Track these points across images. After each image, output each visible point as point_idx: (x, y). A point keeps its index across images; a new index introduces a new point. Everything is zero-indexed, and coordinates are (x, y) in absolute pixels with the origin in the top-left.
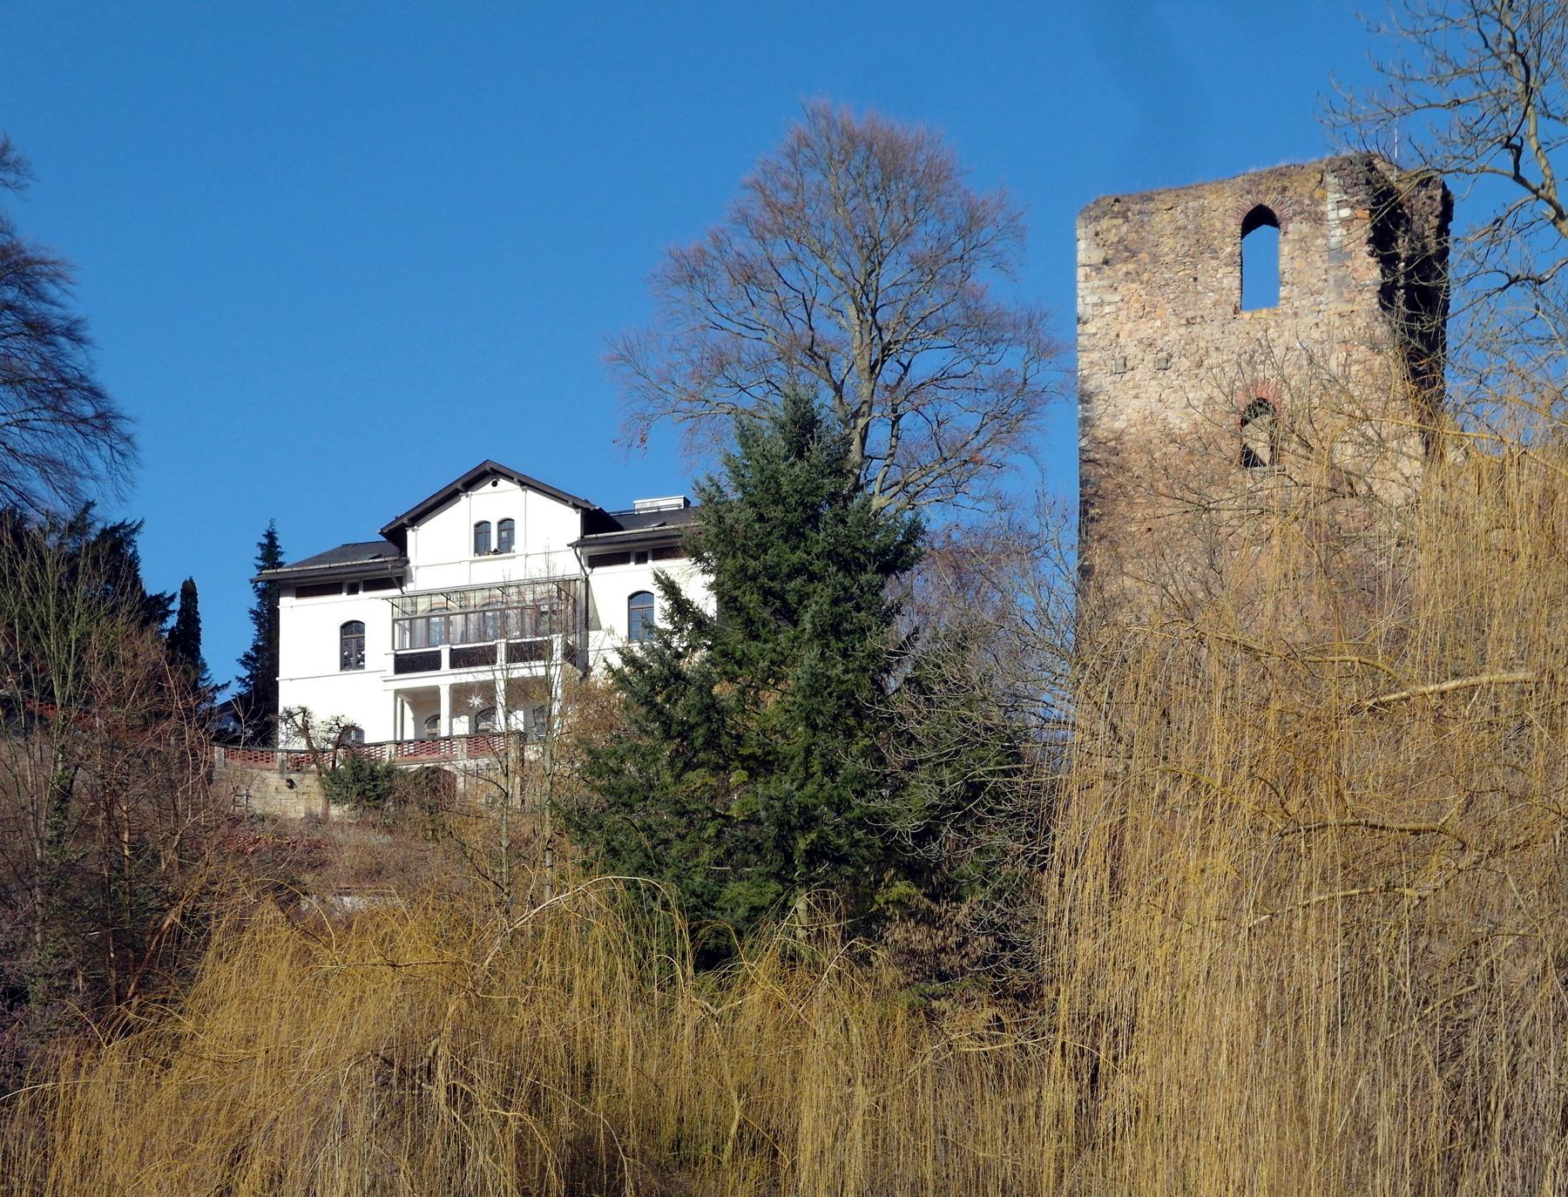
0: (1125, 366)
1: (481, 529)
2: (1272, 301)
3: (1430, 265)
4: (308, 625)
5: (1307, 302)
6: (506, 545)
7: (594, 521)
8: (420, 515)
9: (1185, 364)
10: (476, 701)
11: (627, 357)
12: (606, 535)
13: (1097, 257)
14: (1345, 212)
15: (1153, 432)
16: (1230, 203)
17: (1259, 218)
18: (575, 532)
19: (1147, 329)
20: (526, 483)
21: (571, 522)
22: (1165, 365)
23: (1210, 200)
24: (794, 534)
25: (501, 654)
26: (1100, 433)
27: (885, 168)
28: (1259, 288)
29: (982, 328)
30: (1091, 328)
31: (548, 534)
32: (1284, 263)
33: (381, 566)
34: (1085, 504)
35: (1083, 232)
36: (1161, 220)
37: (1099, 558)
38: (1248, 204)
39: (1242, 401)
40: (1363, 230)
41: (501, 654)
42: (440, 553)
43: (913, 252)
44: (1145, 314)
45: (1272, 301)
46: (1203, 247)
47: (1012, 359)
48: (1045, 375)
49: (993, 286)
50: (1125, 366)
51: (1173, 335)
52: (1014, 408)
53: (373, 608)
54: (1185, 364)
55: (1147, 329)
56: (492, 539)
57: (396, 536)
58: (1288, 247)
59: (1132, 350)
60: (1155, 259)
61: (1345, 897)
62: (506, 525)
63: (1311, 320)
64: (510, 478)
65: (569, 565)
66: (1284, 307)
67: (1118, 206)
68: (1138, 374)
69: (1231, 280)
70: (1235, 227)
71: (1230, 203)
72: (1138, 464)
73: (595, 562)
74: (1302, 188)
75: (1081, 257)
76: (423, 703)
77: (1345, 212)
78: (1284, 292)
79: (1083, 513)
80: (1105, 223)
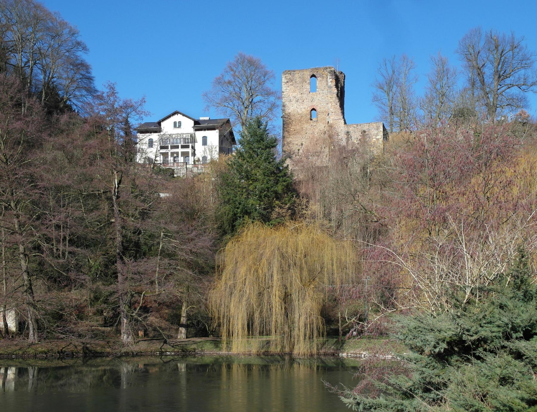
0: (291, 101)
1: (175, 123)
2: (315, 91)
3: (343, 88)
4: (145, 138)
5: (321, 92)
6: (180, 126)
7: (196, 123)
8: (163, 120)
9: (301, 101)
10: (175, 155)
11: (206, 95)
12: (198, 125)
13: (286, 81)
14: (331, 80)
15: (295, 113)
16: (308, 73)
17: (313, 76)
18: (193, 125)
19: (294, 94)
20: (183, 115)
21: (192, 123)
22: (297, 101)
23: (305, 72)
24: (258, 142)
25: (169, 147)
26: (286, 112)
27: (252, 63)
28: (313, 89)
29: (269, 93)
30: (285, 94)
31: (188, 126)
32: (317, 85)
33: (156, 128)
34: (284, 124)
35: (283, 76)
36: (297, 75)
37: (286, 134)
38: (311, 74)
39: (310, 109)
40: (334, 83)
41: (169, 147)
42: (167, 127)
43: (252, 79)
44: (294, 92)
45: (315, 91)
46: (304, 81)
47: (272, 99)
48: (278, 103)
49: (268, 85)
50: (291, 101)
51: (299, 96)
52: (273, 106)
53: (155, 137)
54: (301, 101)
55: (294, 94)
56: (178, 125)
57: (159, 123)
58: (319, 82)
59: (292, 98)
60: (296, 82)
61: (269, 334)
62: (180, 122)
63: (322, 95)
64: (181, 114)
65: (192, 131)
66: (317, 92)
67: (289, 72)
68: (293, 102)
69: (308, 87)
70: (309, 77)
71: (308, 73)
72: (293, 118)
73: (196, 130)
74: (320, 72)
75: (283, 81)
76: (165, 155)
77: (331, 80)
78: (317, 90)
79: (283, 127)
80: (287, 75)
